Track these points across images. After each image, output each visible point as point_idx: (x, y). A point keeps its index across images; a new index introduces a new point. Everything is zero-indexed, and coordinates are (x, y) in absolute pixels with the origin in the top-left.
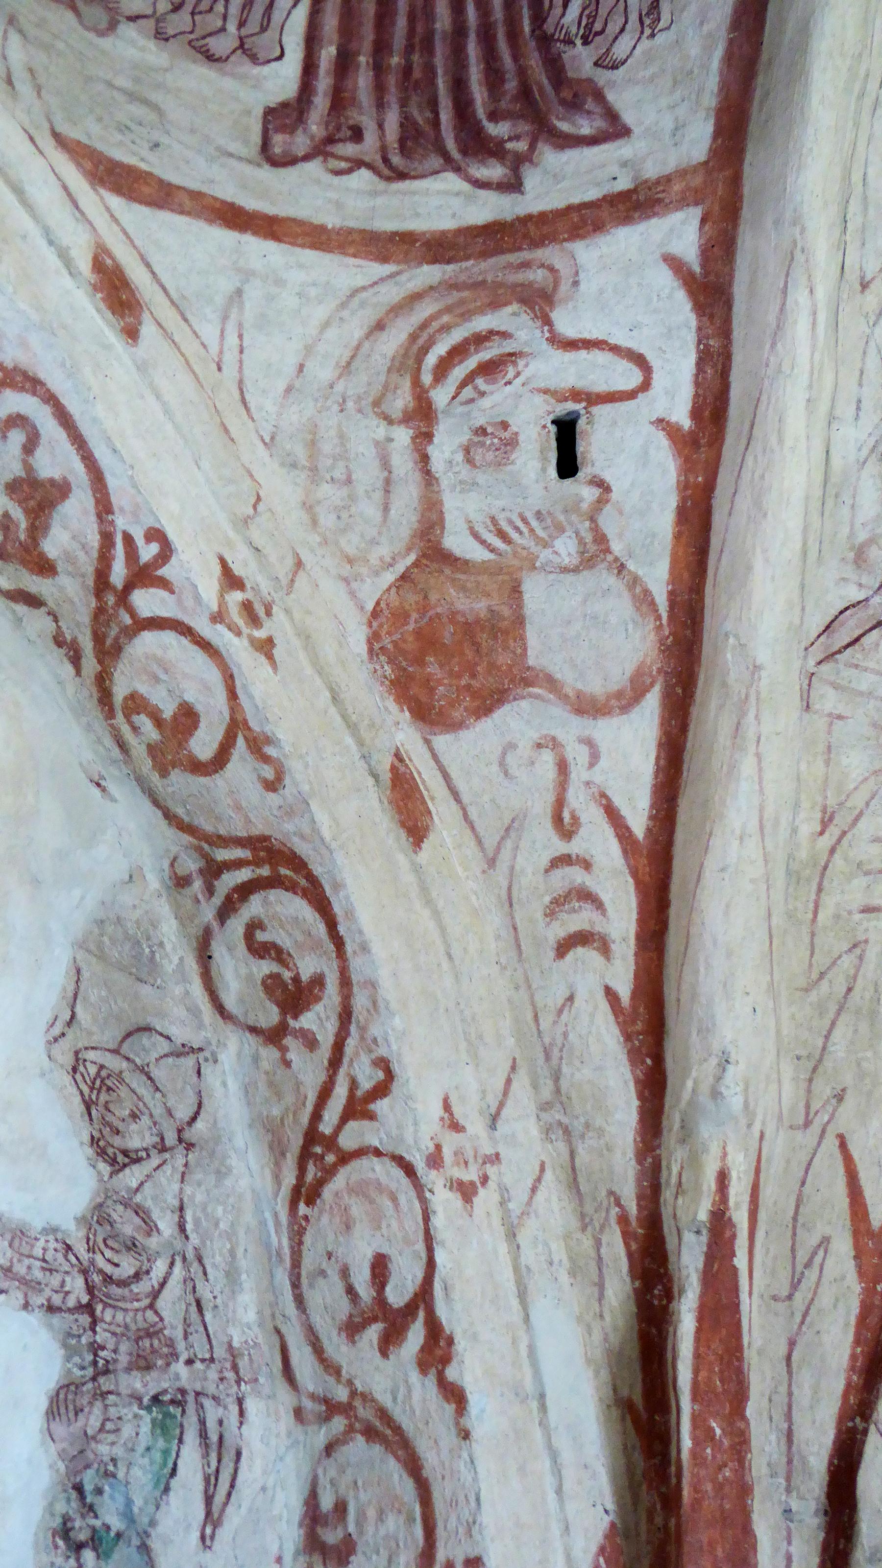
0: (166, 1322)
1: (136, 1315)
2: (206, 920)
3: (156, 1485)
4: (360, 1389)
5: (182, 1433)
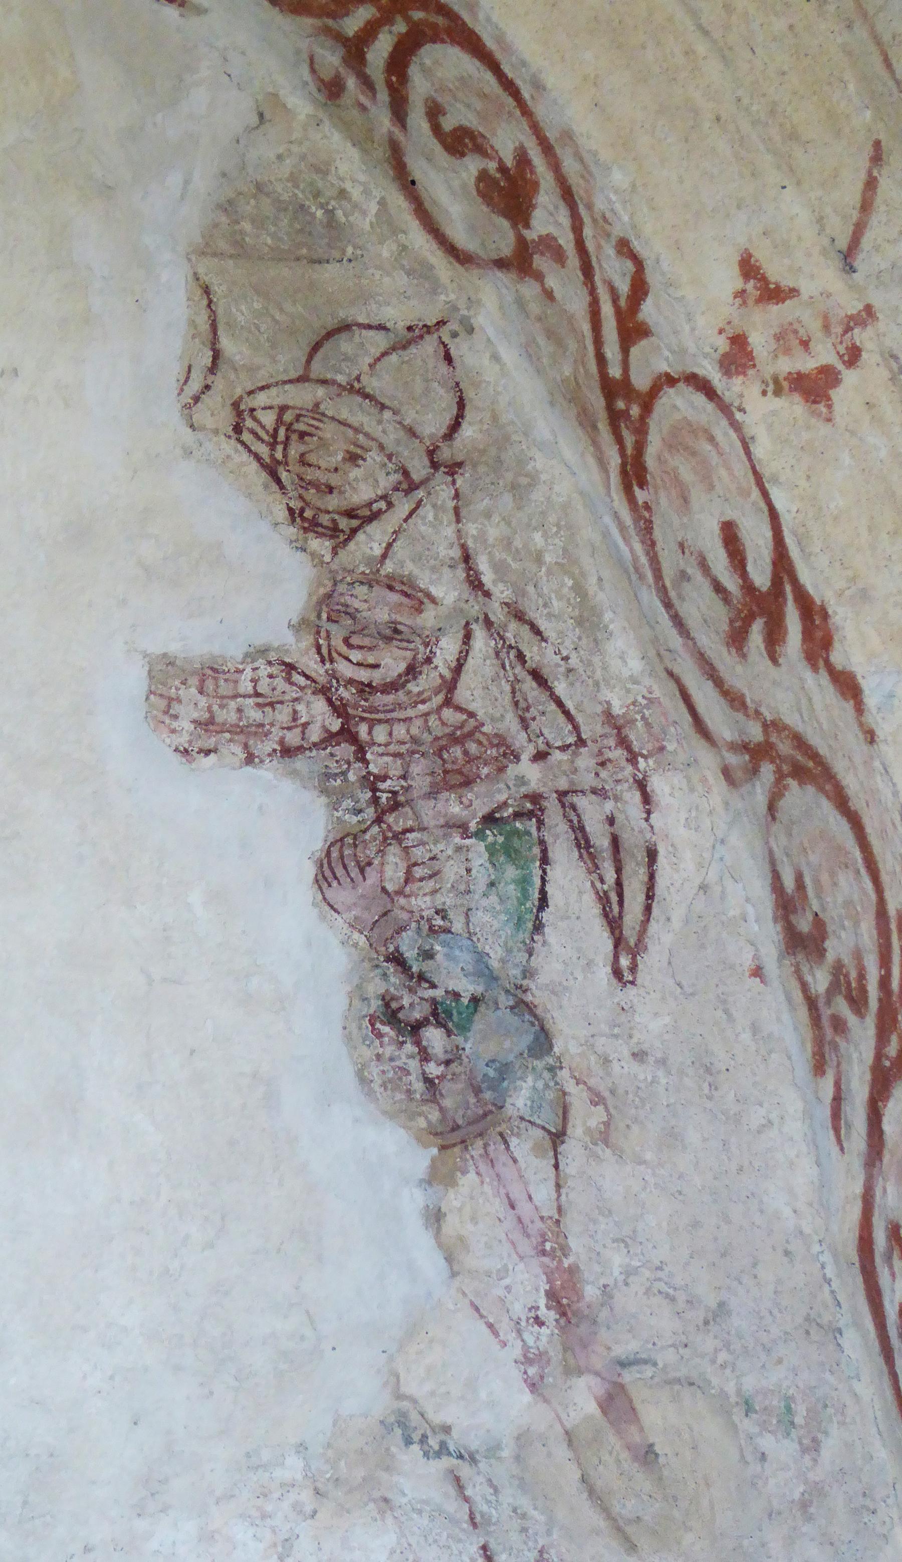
0: (481, 714)
1: (426, 721)
2: (384, 130)
3: (519, 923)
4: (769, 718)
5: (544, 852)
